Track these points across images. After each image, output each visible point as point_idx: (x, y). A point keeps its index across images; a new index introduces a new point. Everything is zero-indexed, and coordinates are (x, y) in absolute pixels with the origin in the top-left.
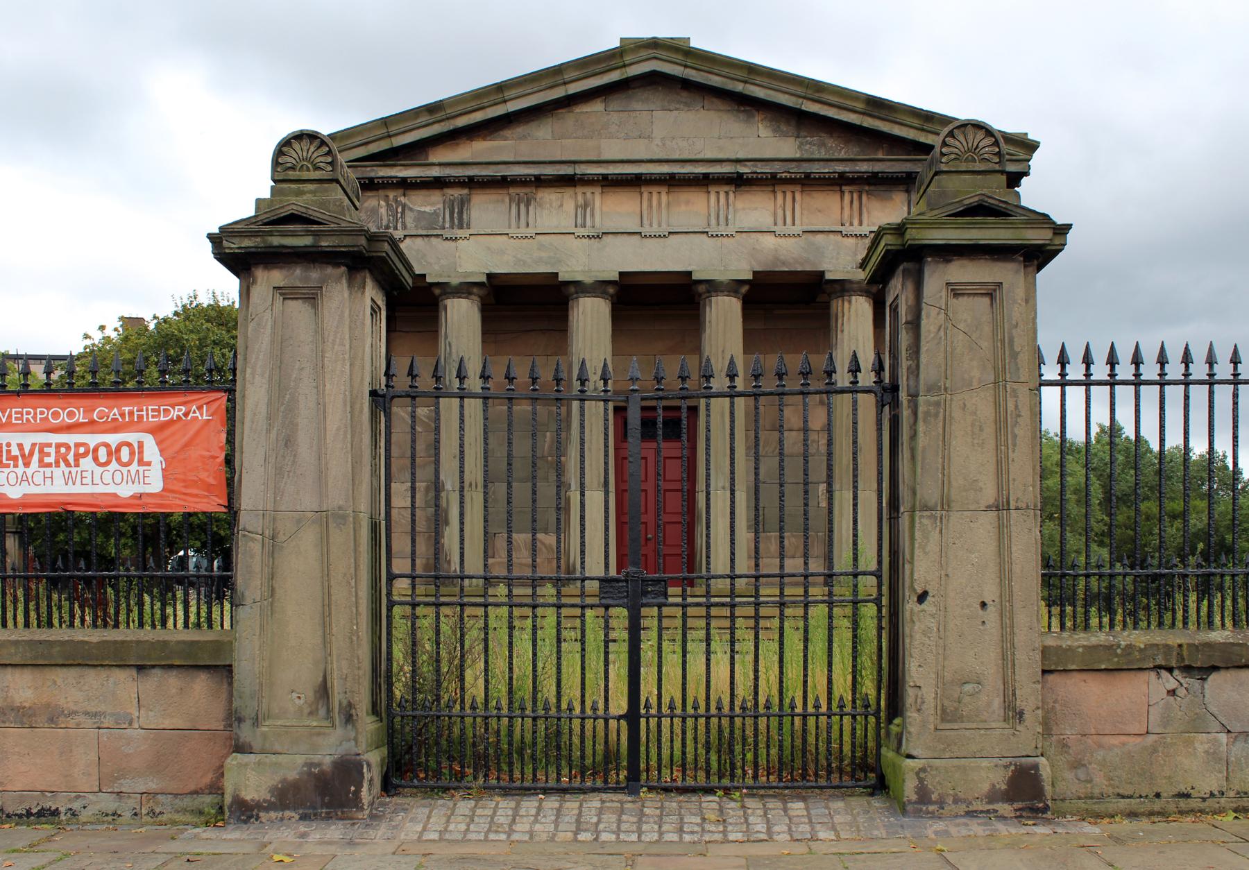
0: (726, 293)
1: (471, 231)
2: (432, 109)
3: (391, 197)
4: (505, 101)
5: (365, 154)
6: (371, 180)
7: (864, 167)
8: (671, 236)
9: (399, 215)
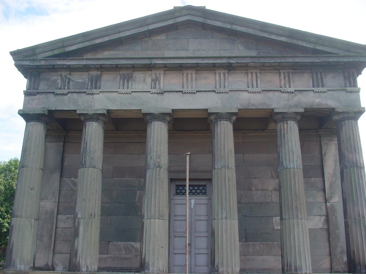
1: (100, 90)
5: (51, 55)
8: (198, 93)
9: (67, 83)
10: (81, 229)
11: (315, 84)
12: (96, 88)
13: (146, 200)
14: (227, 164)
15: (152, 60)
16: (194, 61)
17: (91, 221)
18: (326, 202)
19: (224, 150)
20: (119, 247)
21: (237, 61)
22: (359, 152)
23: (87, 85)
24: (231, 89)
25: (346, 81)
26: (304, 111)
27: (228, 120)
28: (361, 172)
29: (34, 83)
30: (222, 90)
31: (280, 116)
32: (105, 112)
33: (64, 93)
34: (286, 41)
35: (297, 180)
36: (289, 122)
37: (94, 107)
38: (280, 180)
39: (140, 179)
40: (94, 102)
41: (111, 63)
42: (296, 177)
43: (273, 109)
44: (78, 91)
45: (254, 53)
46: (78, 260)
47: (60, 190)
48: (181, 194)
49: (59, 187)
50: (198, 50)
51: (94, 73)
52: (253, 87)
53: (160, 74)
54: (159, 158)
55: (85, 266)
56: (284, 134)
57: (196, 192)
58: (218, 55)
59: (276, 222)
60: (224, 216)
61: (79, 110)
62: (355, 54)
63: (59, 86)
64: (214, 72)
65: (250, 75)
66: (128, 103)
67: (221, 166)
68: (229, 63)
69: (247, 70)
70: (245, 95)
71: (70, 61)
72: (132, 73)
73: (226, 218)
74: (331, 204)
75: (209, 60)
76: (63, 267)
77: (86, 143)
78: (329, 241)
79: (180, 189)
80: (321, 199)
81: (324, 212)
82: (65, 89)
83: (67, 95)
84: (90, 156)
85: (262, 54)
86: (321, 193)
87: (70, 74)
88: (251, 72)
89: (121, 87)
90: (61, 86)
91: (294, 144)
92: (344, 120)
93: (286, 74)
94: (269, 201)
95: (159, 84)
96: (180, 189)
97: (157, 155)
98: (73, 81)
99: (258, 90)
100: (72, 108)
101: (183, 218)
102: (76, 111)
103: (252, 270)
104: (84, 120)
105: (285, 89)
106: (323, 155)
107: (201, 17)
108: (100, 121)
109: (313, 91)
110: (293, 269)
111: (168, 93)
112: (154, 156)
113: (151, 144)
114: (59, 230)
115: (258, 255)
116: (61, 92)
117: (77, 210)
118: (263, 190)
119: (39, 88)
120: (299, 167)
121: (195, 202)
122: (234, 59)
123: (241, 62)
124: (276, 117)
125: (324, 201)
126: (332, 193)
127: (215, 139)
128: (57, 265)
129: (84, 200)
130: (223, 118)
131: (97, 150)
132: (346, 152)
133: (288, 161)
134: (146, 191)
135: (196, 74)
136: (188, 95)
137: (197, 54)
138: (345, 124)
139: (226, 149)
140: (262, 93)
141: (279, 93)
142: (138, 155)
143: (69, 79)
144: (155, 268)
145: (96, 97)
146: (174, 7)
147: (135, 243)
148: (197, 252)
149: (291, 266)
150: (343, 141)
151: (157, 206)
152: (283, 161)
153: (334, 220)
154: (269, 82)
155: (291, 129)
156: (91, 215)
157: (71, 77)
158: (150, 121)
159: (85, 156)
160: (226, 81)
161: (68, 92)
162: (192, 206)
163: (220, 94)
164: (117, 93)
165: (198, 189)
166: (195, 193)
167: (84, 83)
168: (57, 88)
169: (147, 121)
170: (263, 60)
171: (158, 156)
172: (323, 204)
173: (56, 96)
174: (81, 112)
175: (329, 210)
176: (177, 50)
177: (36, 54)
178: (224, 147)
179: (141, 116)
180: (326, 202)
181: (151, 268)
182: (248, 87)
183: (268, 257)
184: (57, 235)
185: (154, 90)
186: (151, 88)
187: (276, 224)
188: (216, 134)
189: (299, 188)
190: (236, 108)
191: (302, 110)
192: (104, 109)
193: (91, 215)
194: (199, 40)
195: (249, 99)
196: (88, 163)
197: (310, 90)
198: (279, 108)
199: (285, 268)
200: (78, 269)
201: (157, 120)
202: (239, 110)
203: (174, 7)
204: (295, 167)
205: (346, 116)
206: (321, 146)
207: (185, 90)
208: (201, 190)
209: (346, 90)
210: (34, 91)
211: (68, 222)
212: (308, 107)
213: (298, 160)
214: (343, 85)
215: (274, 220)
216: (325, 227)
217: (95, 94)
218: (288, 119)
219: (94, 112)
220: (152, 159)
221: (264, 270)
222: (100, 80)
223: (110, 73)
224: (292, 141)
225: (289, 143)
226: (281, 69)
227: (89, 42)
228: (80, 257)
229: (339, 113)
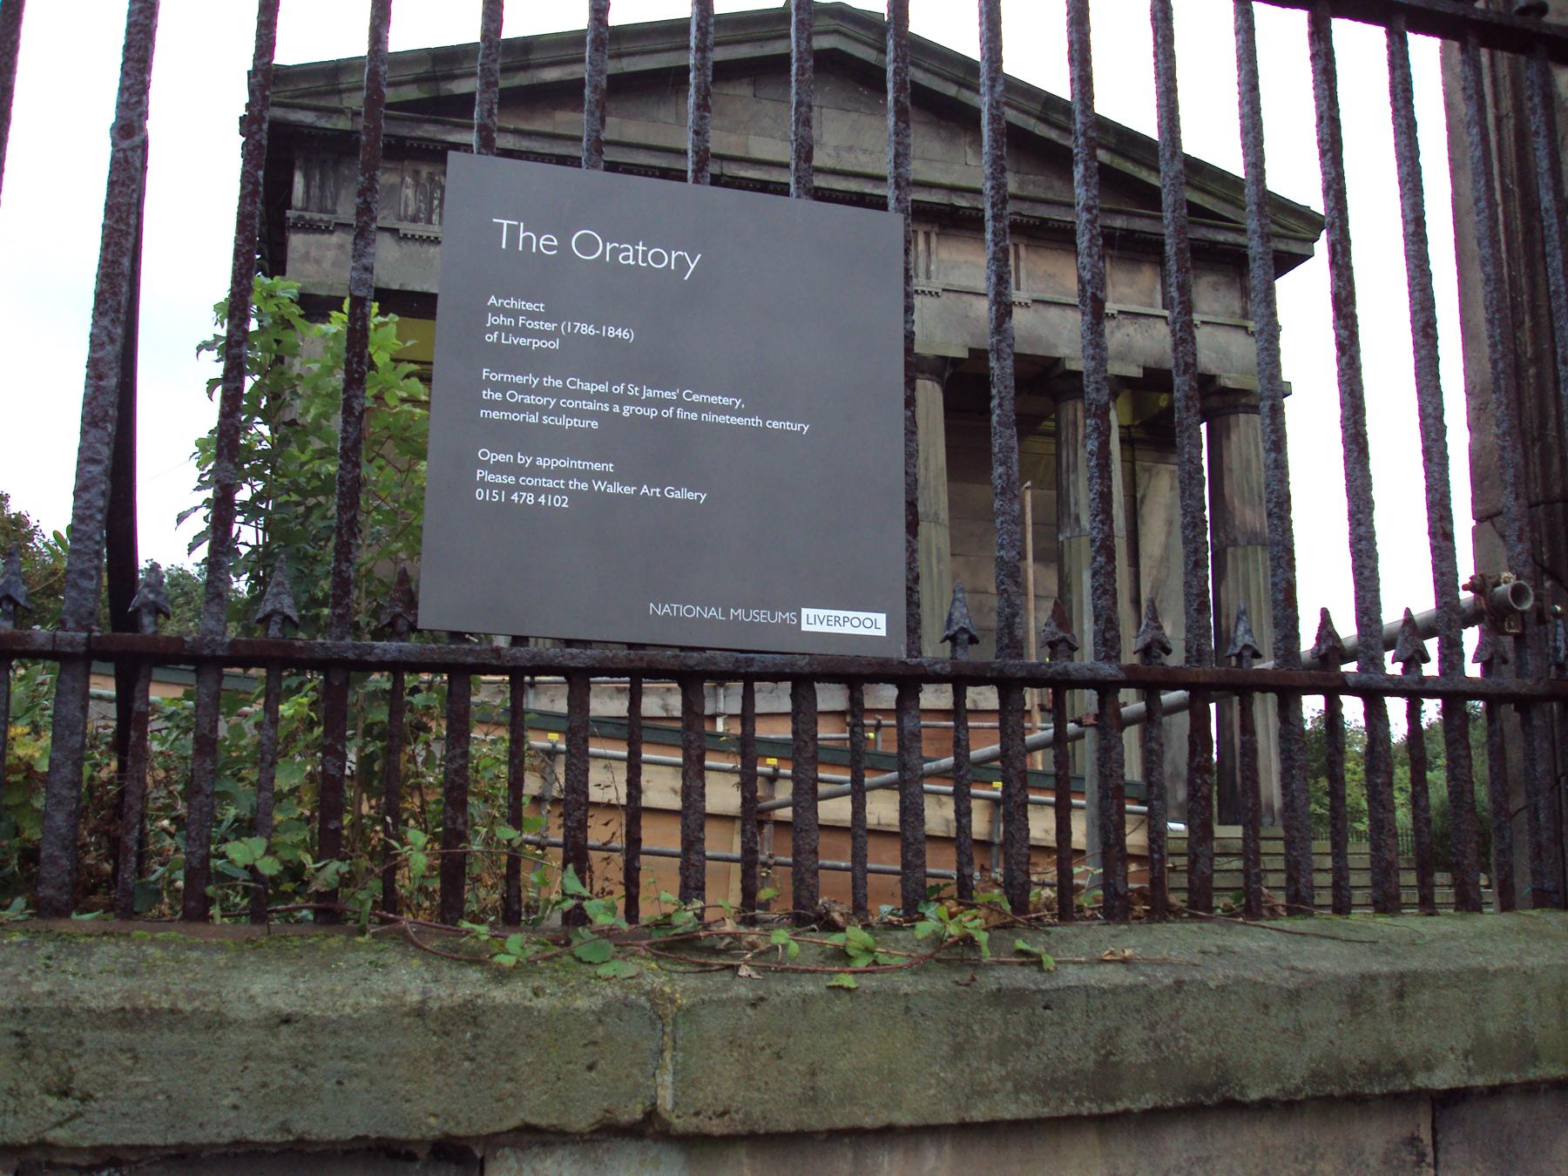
0: (927, 375)
3: (424, 174)
6: (401, 140)
9: (436, 202)
26: (1141, 375)
29: (322, 187)
34: (1108, 162)
50: (850, 149)
62: (1281, 231)
63: (411, 211)
82: (429, 221)
90: (418, 210)
107: (870, 46)
109: (1163, 321)
116: (419, 229)
118: (975, 591)
119: (339, 210)
132: (1237, 502)
137: (849, 163)
150: (1231, 470)
160: (933, 257)
168: (406, 217)
173: (403, 243)
177: (340, 92)
194: (854, 115)
202: (971, 350)
209: (1246, 328)
210: (325, 217)
212: (1151, 364)
214: (1238, 311)
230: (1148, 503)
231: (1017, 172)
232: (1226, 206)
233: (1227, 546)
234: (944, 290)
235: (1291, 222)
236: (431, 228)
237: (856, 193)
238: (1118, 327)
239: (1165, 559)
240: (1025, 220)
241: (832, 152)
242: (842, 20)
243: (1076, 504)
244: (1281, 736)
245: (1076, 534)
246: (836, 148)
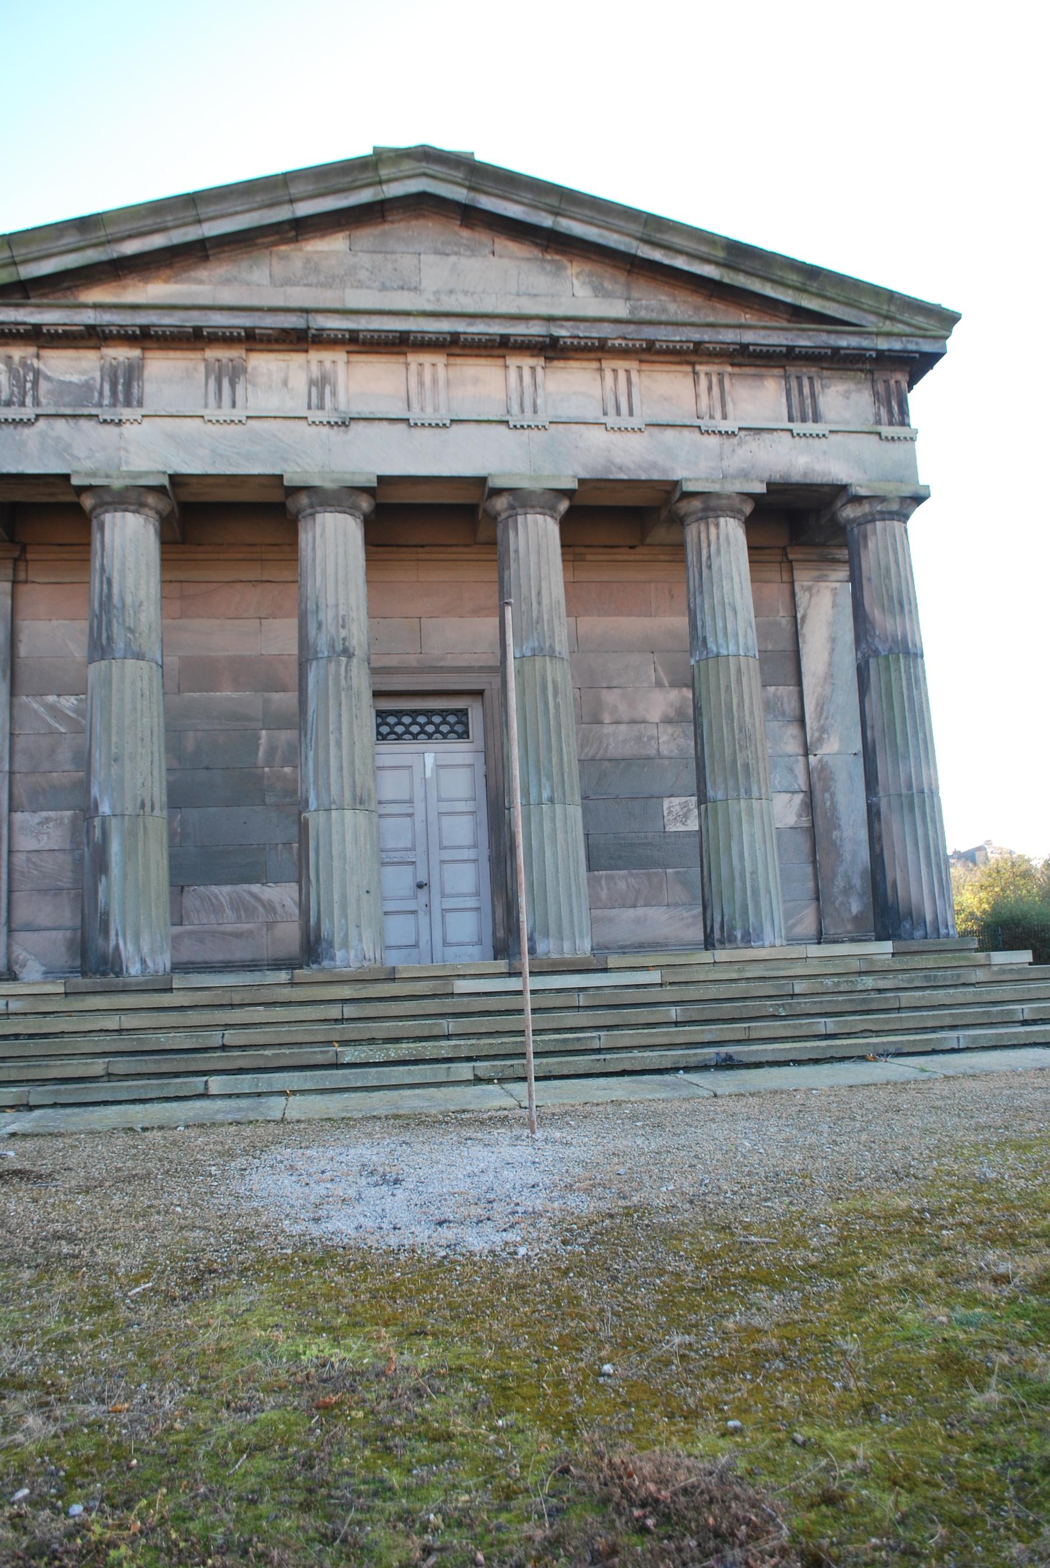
2: (84, 224)
4: (199, 222)
7: (729, 336)
8: (455, 427)
10: (115, 848)
11: (796, 413)
12: (128, 404)
13: (311, 754)
14: (547, 644)
15: (311, 317)
16: (445, 326)
17: (144, 824)
18: (806, 755)
19: (539, 603)
20: (214, 901)
21: (576, 332)
22: (910, 612)
23: (96, 394)
24: (555, 417)
25: (879, 408)
27: (547, 511)
28: (915, 667)
30: (528, 419)
31: (696, 504)
32: (165, 481)
33: (21, 420)
35: (746, 689)
36: (722, 520)
37: (127, 463)
38: (697, 693)
39: (266, 694)
40: (126, 450)
41: (178, 323)
42: (745, 680)
43: (676, 483)
44: (68, 411)
45: (619, 309)
46: (112, 943)
47: (12, 734)
48: (394, 736)
49: (8, 726)
51: (121, 354)
52: (618, 413)
53: (334, 362)
54: (343, 627)
55: (137, 959)
56: (709, 557)
57: (437, 731)
58: (512, 310)
59: (669, 813)
60: (546, 794)
61: (77, 472)
64: (500, 362)
65: (609, 376)
66: (238, 454)
67: (533, 649)
68: (551, 337)
69: (600, 360)
70: (597, 437)
71: (40, 313)
72: (244, 356)
73: (551, 800)
74: (821, 760)
75: (489, 326)
76: (43, 968)
77: (109, 583)
78: (814, 862)
79: (388, 724)
80: (793, 747)
81: (802, 782)
82: (23, 404)
83: (33, 424)
84: (124, 621)
85: (643, 314)
86: (793, 730)
87: (38, 357)
88: (615, 367)
89: (212, 400)
90: (12, 394)
91: (737, 586)
92: (873, 520)
93: (715, 379)
94: (653, 752)
95: (334, 394)
96: (388, 724)
97: (337, 616)
98: (48, 378)
99: (636, 422)
100: (54, 467)
101: (404, 809)
102: (66, 477)
103: (608, 948)
104: (94, 509)
105: (713, 421)
106: (799, 621)
108: (146, 510)
109: (789, 434)
110: (739, 935)
111: (362, 424)
112: (330, 620)
113: (318, 584)
114: (19, 859)
115: (624, 906)
117: (95, 791)
118: (633, 722)
120: (751, 653)
121: (435, 760)
122: (565, 323)
123: (587, 334)
124: (684, 507)
125: (801, 751)
126: (823, 730)
127: (509, 567)
128: (24, 966)
129: (115, 760)
130: (533, 507)
131: (145, 603)
133: (720, 634)
134: (309, 729)
135: (446, 366)
136: (428, 432)
137: (450, 304)
138: (875, 533)
139: (545, 601)
140: (646, 433)
141: (696, 435)
142: (258, 621)
143: (37, 373)
144: (352, 953)
145: (127, 428)
146: (375, 148)
147: (265, 888)
148: (448, 904)
149: (733, 928)
151: (345, 773)
152: (708, 635)
153: (828, 804)
154: (665, 399)
155: (729, 544)
156: (143, 805)
157: (42, 367)
158: (309, 511)
159: (109, 623)
160: (540, 391)
161: (38, 416)
162: (428, 774)
163: (522, 431)
164: (198, 421)
165: (414, 723)
166: (434, 733)
167: (87, 386)
169: (298, 513)
170: (649, 332)
171: (340, 619)
172: (797, 761)
174: (86, 482)
175: (815, 776)
176: (384, 288)
178: (539, 594)
179: (276, 496)
180: (806, 755)
181: (339, 954)
182: (605, 414)
183: (651, 911)
184: (17, 876)
185: (319, 413)
186: (309, 408)
187: (671, 817)
188: (512, 555)
189: (752, 713)
190: (575, 477)
191: (762, 488)
192: (159, 472)
193: (143, 805)
194: (453, 259)
195: (609, 451)
196: (120, 645)
197: (782, 430)
198: (697, 480)
199: (717, 934)
200: (117, 969)
201: (332, 509)
202: (581, 481)
203: (375, 148)
204: (742, 653)
205: (879, 508)
206: (793, 595)
207: (414, 416)
208: (437, 726)
209: (879, 434)
211: (48, 833)
212: (777, 478)
213: (749, 630)
215: (665, 807)
216: (805, 822)
217: (128, 425)
218: (720, 513)
219: (129, 482)
220: (324, 626)
221: (640, 947)
222: (140, 377)
223: (172, 354)
224: (732, 578)
225: (724, 583)
226: (701, 363)
227: (101, 249)
228: (117, 931)
229: (858, 499)
230: (809, 623)
231: (628, 299)
232: (847, 310)
233: (869, 656)
234: (551, 423)
235: (920, 320)
236: (23, 410)
237: (449, 333)
238: (740, 444)
239: (830, 676)
240: (630, 344)
241: (432, 298)
242: (428, 162)
243: (703, 626)
244: (590, 896)
245: (704, 657)
246: (437, 293)
